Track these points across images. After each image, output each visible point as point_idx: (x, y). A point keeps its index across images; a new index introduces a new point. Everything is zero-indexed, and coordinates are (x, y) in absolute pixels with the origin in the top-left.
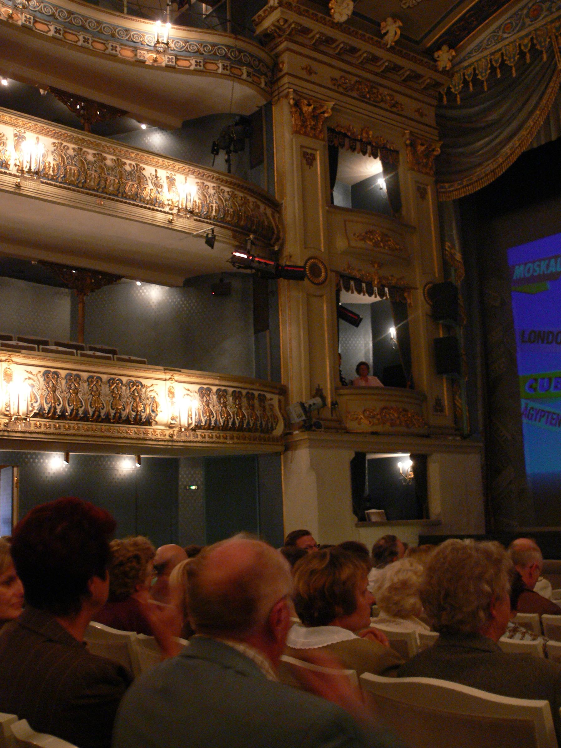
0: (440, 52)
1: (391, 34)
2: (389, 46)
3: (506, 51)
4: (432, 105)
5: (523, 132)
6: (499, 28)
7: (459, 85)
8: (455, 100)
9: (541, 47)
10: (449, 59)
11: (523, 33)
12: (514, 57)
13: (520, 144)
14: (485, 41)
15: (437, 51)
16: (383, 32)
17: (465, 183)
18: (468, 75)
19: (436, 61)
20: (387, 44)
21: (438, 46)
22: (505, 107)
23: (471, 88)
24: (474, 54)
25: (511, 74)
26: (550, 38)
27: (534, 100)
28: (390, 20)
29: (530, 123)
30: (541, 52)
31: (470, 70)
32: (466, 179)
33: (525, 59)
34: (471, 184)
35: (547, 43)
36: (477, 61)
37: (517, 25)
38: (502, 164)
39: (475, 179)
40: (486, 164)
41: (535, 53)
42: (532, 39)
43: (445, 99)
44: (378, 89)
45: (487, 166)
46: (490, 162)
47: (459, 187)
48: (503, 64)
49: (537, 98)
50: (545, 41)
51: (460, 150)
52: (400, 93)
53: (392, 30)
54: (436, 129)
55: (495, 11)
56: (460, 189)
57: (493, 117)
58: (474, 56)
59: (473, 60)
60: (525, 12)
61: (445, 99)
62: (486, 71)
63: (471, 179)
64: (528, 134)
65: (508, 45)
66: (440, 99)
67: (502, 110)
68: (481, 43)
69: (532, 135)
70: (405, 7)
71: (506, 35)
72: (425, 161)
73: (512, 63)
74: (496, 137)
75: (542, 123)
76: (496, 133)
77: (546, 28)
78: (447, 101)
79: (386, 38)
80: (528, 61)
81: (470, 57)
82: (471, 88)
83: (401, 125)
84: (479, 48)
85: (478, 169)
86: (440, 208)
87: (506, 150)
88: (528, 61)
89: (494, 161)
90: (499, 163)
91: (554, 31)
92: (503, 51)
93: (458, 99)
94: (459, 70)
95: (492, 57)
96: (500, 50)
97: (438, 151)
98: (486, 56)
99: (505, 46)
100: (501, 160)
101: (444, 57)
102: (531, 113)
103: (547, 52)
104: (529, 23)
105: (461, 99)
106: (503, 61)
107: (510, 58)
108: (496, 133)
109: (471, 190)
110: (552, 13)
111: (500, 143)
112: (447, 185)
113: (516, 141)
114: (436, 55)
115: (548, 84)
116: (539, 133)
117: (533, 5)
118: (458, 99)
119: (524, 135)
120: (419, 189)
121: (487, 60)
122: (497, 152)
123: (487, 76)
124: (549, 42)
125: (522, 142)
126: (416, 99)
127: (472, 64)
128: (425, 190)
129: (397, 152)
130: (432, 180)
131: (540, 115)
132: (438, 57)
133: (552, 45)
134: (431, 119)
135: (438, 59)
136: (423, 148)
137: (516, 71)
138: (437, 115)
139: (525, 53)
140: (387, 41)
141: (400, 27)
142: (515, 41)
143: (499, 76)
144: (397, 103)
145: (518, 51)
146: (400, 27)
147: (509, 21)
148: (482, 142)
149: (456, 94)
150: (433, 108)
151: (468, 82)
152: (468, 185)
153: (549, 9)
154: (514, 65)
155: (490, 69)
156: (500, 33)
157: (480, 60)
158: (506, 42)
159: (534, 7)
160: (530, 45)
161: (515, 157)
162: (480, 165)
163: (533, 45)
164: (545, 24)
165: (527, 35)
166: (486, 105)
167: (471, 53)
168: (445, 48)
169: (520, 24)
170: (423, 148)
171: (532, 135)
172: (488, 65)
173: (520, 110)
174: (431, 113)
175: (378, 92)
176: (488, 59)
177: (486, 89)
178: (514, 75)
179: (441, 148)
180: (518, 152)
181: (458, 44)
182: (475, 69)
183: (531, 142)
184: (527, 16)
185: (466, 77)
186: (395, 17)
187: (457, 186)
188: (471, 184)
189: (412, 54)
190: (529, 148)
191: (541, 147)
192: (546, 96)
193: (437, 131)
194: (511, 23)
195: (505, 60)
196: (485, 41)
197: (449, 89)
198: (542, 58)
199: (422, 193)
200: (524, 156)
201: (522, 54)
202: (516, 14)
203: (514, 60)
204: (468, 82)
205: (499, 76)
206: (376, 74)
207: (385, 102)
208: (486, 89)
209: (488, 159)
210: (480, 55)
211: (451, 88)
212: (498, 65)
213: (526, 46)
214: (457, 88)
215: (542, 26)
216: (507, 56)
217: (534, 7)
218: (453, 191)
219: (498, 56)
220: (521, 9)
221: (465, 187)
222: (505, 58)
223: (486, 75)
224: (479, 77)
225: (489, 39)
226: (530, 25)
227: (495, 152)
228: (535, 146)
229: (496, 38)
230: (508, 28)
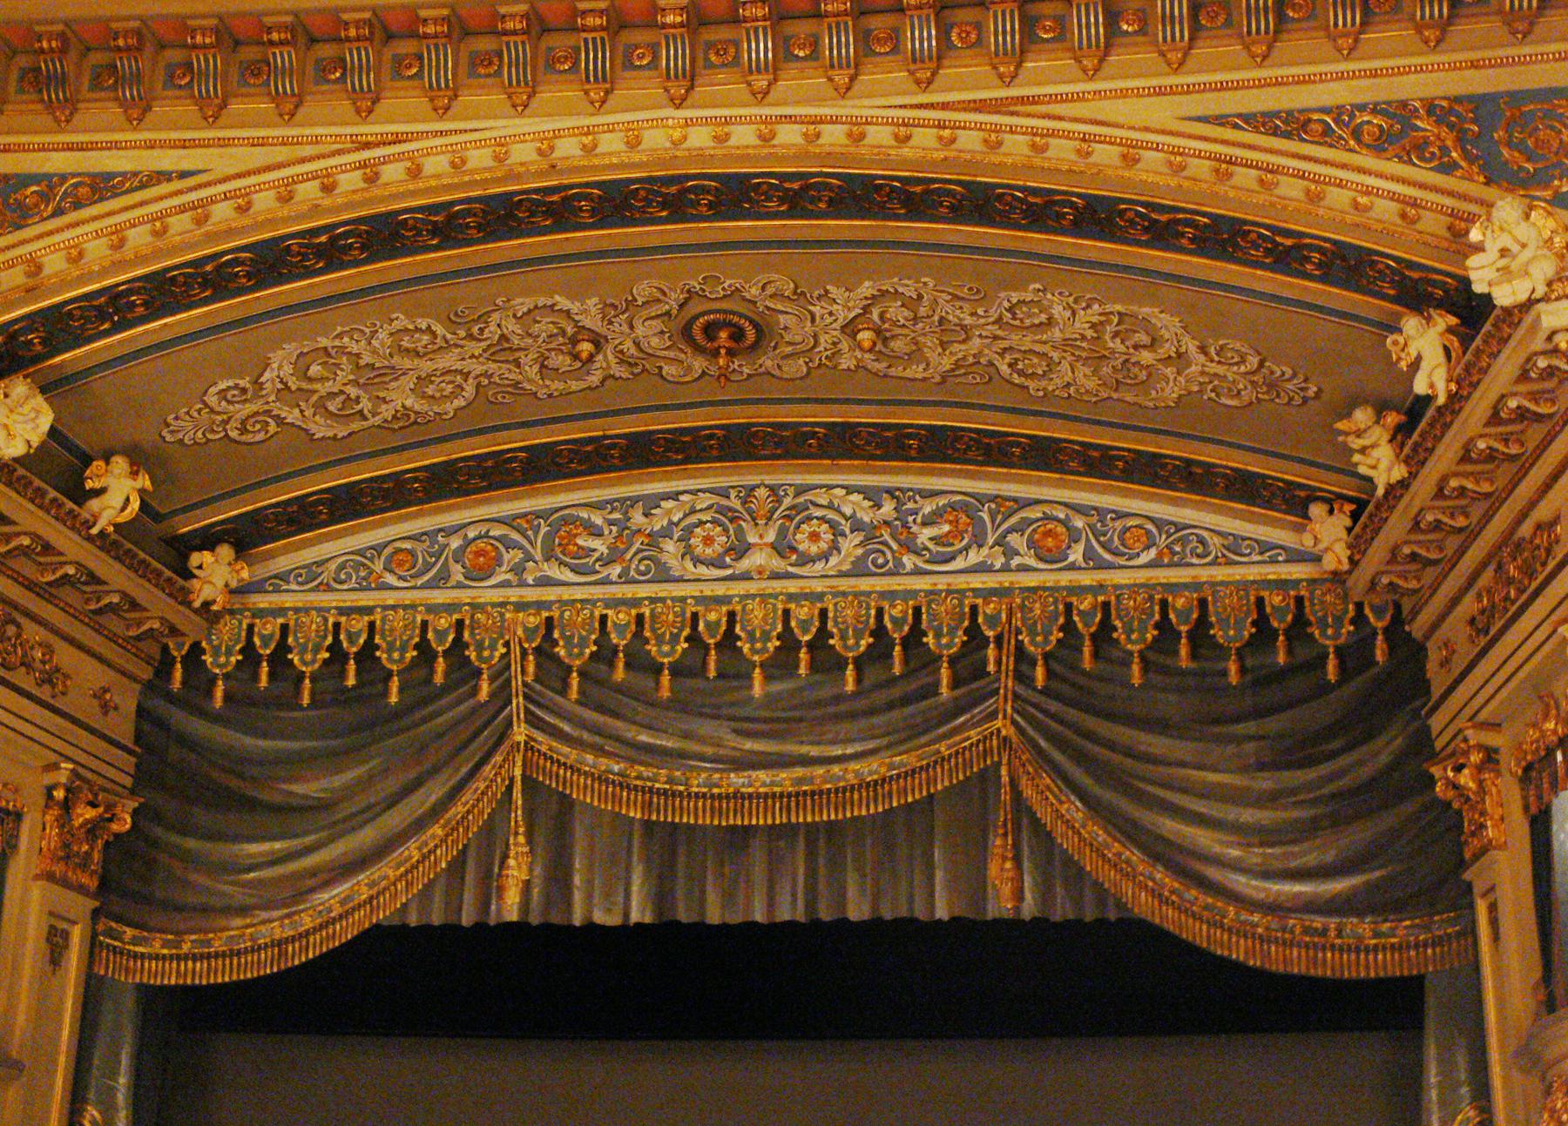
0: (206, 557)
1: (114, 499)
2: (94, 531)
3: (383, 620)
4: (133, 678)
5: (386, 870)
6: (378, 549)
7: (229, 653)
8: (209, 693)
9: (480, 657)
10: (227, 585)
11: (439, 597)
12: (403, 650)
13: (371, 898)
14: (333, 566)
15: (200, 549)
16: (89, 485)
17: (186, 948)
18: (262, 637)
19: (188, 575)
20: (94, 524)
21: (208, 540)
22: (349, 776)
23: (264, 681)
24: (294, 587)
25: (385, 693)
26: (507, 644)
27: (434, 791)
28: (120, 464)
29: (412, 850)
30: (478, 673)
31: (271, 627)
32: (193, 937)
33: (432, 671)
34: (202, 957)
35: (497, 654)
36: (296, 610)
37: (428, 567)
38: (307, 933)
39: (218, 946)
40: (264, 915)
41: (464, 671)
42: (460, 624)
43: (178, 674)
44: (18, 626)
45: (264, 922)
46: (276, 914)
47: (165, 951)
48: (367, 654)
49: (446, 789)
50: (493, 648)
51: (192, 844)
52: (71, 641)
53: (118, 493)
54: (130, 752)
55: (383, 511)
56: (166, 960)
57: (310, 788)
58: (287, 591)
59: (288, 601)
60: (455, 543)
61: (178, 674)
62: (316, 650)
63: (208, 943)
64: (399, 879)
65: (394, 608)
66: (164, 667)
67: (338, 781)
68: (319, 564)
69: (409, 885)
70: (169, 438)
71: (390, 579)
72: (85, 848)
73: (395, 661)
74: (308, 850)
75: (444, 865)
76: (309, 840)
77: (502, 615)
78: (184, 683)
79: (94, 504)
80: (439, 678)
81: (277, 590)
82: (264, 681)
83: (58, 744)
84: (310, 575)
85: (238, 922)
86: (93, 993)
87: (330, 897)
88: (439, 678)
89: (288, 916)
90: (301, 929)
91: (520, 632)
92: (377, 617)
93: (219, 693)
94: (241, 611)
95: (343, 619)
96: (369, 610)
97: (124, 824)
98: (328, 610)
99: (385, 608)
100: (307, 922)
101: (215, 572)
102: (420, 825)
103: (492, 680)
104: (461, 578)
105: (227, 697)
106: (370, 646)
107: (391, 648)
108: (309, 840)
109: (199, 974)
110: (523, 584)
111: (313, 872)
112: (130, 932)
113: (359, 885)
114: (195, 558)
115: (478, 767)
116: (429, 886)
117: (479, 537)
118: (219, 693)
119: (386, 877)
120: (53, 932)
121: (326, 620)
122: (301, 896)
123: (317, 666)
124: (503, 656)
125: (378, 894)
126: (100, 658)
127: (282, 611)
128: (66, 935)
129: (18, 816)
130: (82, 906)
131: (444, 840)
132: (200, 567)
133: (508, 666)
134: (123, 726)
135: (196, 572)
136: (90, 813)
137: (401, 690)
138: (141, 712)
139: (435, 655)
140: (96, 518)
141: (142, 492)
142: (413, 607)
143: (351, 681)
144: (58, 670)
145: (417, 639)
146: (142, 492)
147: (407, 545)
148: (266, 847)
149: (215, 677)
150: (138, 687)
151: (258, 659)
152: (195, 958)
153: (518, 570)
154: (400, 673)
155: (329, 649)
156: (378, 566)
157: (307, 610)
158: (390, 598)
159: (481, 544)
160: (451, 637)
161: (346, 932)
162: (243, 911)
163: (459, 643)
164: (503, 604)
165: (450, 608)
166: (295, 745)
167: (283, 577)
168: (225, 551)
169: (434, 570)
170: (90, 813)
171: (409, 885)
172: (325, 637)
173: (393, 802)
174: (127, 700)
175: (19, 636)
176: (331, 621)
177: (306, 701)
178: (394, 699)
179: (135, 814)
180: (361, 921)
181: (256, 546)
182: (285, 629)
183: (404, 905)
184: (458, 556)
185: (257, 641)
186: (139, 459)
187: (157, 947)
188: (202, 957)
189: (142, 555)
190: (396, 922)
191: (426, 930)
192: (468, 796)
193: (134, 760)
194: (411, 553)
195: (377, 647)
196: (333, 566)
197: (196, 649)
198: (475, 691)
199: (56, 942)
200: (376, 935)
201: (425, 652)
202: (431, 535)
203: (402, 657)
204: (258, 659)
205: (351, 681)
206: (30, 586)
207: (27, 664)
208: (306, 701)
209: (268, 906)
210: (312, 597)
211: (203, 652)
212: (354, 649)
213: (441, 635)
214: (222, 659)
215: (494, 605)
216: (383, 637)
217: (481, 544)
218: (142, 956)
219: (359, 624)
220: (451, 531)
221: (179, 958)
222: (377, 640)
223: (314, 661)
224: (294, 658)
225: (342, 567)
226: (459, 586)
227: (297, 891)
228: (413, 920)
229: (363, 574)
230: (400, 564)
